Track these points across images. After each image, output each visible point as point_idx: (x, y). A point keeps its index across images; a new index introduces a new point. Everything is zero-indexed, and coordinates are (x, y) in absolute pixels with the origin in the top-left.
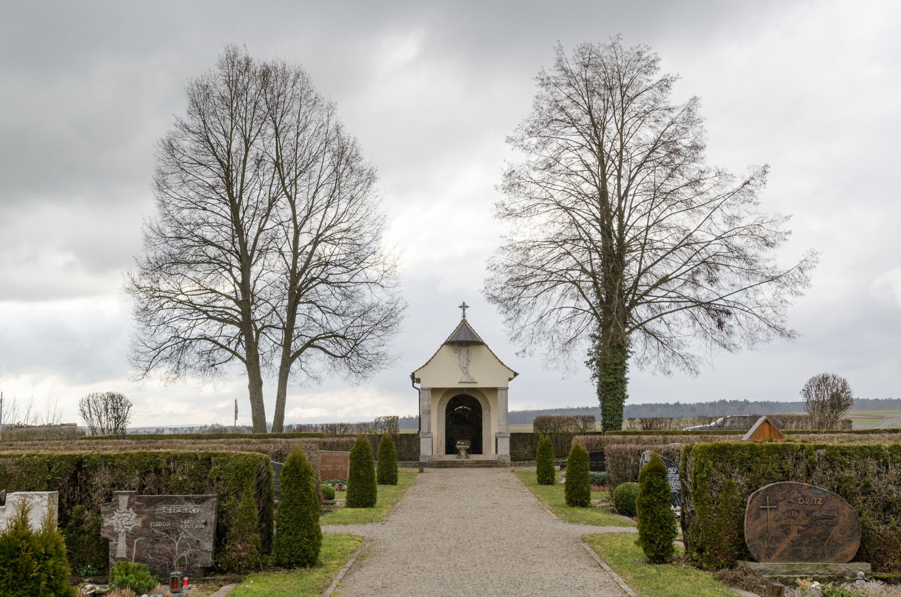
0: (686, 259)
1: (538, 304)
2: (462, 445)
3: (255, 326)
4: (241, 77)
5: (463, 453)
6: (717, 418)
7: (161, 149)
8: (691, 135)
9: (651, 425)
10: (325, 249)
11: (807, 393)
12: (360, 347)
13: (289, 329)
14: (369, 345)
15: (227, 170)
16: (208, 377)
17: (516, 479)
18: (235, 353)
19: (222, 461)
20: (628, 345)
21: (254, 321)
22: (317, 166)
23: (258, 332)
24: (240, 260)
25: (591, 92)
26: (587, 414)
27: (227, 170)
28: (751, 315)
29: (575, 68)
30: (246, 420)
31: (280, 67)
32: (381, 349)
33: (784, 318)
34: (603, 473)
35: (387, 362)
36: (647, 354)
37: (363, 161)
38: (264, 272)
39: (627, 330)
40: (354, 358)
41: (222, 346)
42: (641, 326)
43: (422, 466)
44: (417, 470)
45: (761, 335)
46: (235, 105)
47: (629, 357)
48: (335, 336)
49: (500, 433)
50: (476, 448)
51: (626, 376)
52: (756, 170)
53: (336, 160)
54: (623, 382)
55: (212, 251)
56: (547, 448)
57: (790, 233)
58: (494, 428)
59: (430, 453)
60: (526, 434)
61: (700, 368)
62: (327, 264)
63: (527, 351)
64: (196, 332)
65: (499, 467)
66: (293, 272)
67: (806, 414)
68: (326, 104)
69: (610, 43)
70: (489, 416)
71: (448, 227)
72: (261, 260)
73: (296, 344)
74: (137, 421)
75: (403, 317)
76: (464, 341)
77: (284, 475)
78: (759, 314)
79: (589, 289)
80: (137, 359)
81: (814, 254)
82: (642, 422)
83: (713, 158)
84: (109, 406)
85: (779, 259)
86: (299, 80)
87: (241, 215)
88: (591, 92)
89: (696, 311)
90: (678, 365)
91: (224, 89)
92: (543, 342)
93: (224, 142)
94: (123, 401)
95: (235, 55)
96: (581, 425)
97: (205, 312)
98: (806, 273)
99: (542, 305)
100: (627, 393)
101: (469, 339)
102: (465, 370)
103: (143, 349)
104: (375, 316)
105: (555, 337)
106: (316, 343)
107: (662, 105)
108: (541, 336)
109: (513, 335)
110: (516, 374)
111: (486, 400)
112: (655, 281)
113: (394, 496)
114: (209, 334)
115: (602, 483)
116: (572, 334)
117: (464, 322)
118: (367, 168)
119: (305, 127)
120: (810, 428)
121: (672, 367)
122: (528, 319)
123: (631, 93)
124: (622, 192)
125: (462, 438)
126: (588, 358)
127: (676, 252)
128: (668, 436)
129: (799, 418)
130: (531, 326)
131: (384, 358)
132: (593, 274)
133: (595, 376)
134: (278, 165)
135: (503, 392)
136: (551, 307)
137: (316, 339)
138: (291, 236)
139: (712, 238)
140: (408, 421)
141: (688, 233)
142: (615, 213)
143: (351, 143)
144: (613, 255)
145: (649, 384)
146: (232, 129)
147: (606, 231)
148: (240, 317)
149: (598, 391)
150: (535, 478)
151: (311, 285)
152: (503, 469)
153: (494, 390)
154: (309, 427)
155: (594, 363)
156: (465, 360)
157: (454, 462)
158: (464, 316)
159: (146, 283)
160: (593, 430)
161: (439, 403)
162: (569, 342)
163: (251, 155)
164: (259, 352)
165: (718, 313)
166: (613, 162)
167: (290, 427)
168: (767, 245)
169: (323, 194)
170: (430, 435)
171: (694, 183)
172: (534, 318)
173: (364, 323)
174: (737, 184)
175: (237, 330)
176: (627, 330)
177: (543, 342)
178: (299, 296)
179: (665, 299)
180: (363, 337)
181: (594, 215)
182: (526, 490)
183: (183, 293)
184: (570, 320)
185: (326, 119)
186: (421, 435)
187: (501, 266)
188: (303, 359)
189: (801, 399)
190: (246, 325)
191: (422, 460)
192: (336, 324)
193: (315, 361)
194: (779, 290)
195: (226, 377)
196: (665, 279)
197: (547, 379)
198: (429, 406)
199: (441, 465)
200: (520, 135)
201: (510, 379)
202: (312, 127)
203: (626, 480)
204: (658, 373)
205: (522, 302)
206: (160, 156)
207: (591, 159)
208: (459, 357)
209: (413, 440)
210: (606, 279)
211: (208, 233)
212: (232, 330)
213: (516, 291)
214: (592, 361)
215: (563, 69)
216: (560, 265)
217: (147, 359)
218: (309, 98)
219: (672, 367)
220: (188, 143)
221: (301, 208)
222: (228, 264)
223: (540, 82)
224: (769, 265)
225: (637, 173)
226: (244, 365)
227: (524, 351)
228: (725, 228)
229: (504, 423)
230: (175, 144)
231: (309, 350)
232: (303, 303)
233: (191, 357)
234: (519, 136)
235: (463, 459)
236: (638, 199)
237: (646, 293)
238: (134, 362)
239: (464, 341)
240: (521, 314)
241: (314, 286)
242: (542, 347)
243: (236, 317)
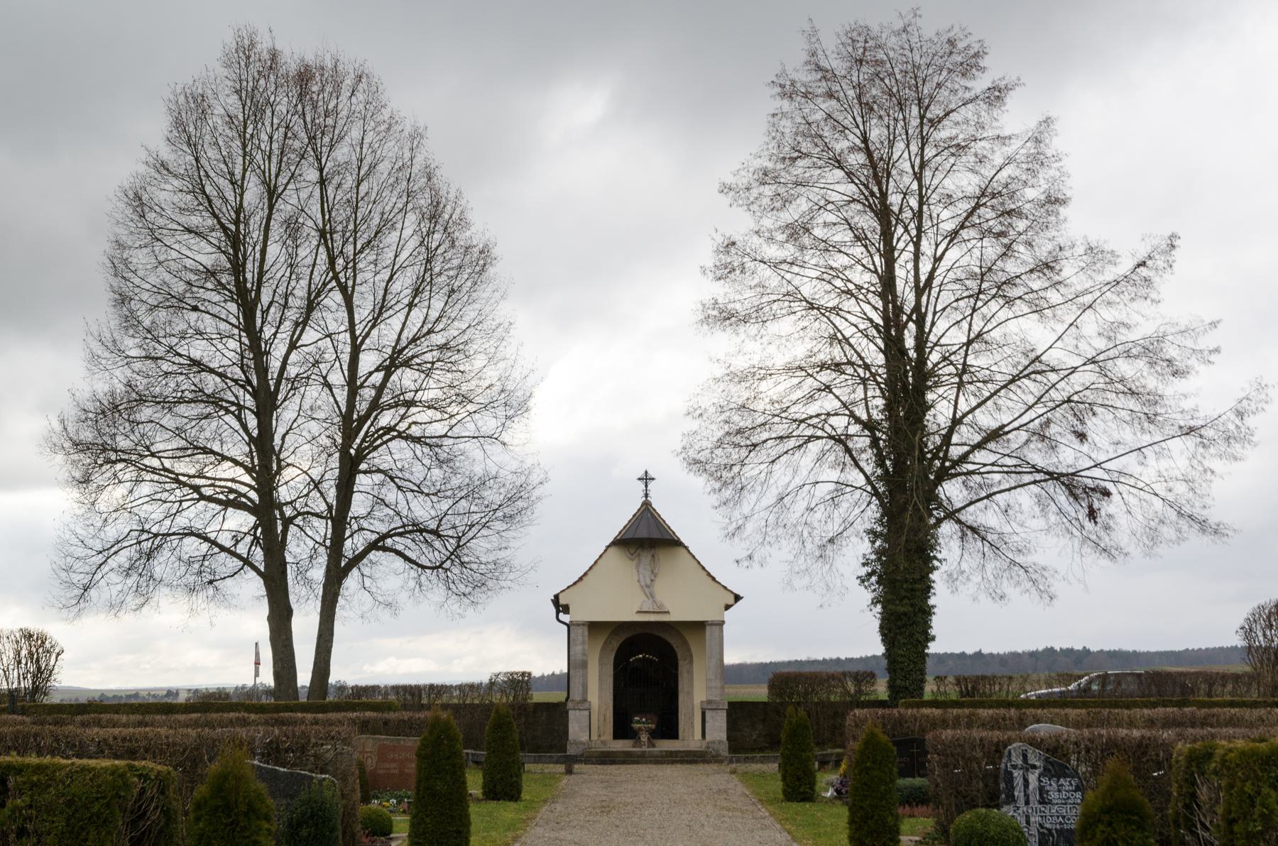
0: (1031, 400)
1: (775, 476)
2: (641, 723)
3: (282, 513)
4: (262, 82)
5: (644, 738)
6: (1080, 677)
7: (122, 205)
8: (1042, 182)
9: (973, 688)
10: (405, 378)
11: (1248, 632)
12: (466, 551)
13: (339, 517)
14: (481, 547)
15: (236, 241)
16: (200, 600)
17: (741, 788)
18: (247, 562)
19: (34, 785)
20: (932, 548)
21: (280, 506)
22: (392, 238)
23: (288, 522)
24: (254, 395)
25: (867, 108)
26: (861, 668)
27: (236, 241)
28: (1147, 496)
29: (839, 66)
30: (267, 678)
31: (329, 64)
32: (502, 554)
33: (1208, 501)
34: (918, 781)
35: (511, 576)
36: (964, 566)
37: (473, 229)
38: (300, 421)
39: (932, 521)
40: (456, 570)
41: (223, 549)
42: (952, 515)
43: (569, 762)
44: (561, 768)
45: (1167, 532)
46: (250, 130)
47: (936, 568)
48: (421, 531)
49: (709, 702)
50: (668, 727)
51: (931, 602)
52: (1155, 242)
53: (425, 227)
54: (926, 612)
55: (211, 383)
56: (790, 721)
57: (1217, 350)
58: (698, 691)
59: (585, 738)
60: (755, 704)
61: (1057, 587)
62: (410, 404)
63: (756, 557)
64: (181, 521)
65: (708, 762)
66: (346, 418)
67: (1248, 669)
68: (408, 129)
69: (899, 25)
70: (690, 672)
71: (626, 381)
72: (297, 399)
73: (353, 544)
74: (77, 675)
75: (539, 498)
76: (647, 539)
77: (198, 819)
78: (1162, 493)
79: (864, 451)
80: (68, 569)
81: (1261, 387)
82: (958, 682)
83: (1076, 225)
84: (24, 652)
85: (1203, 392)
86: (361, 87)
87: (259, 322)
88: (867, 108)
89: (1050, 486)
90: (1018, 583)
91: (233, 103)
92: (784, 542)
93: (230, 195)
94: (47, 645)
95: (252, 45)
96: (851, 687)
97: (196, 489)
98: (1250, 421)
99: (782, 476)
100: (933, 632)
101: (656, 535)
102: (648, 590)
103: (80, 552)
104: (492, 496)
105: (806, 534)
106: (389, 542)
107: (990, 133)
108: (780, 531)
109: (732, 528)
110: (737, 598)
111: (685, 643)
112: (977, 438)
113: (511, 827)
114: (198, 525)
115: (917, 799)
116: (834, 528)
117: (646, 507)
118: (478, 241)
119: (372, 167)
120: (1254, 696)
121: (1007, 587)
122: (757, 503)
123: (935, 111)
124: (923, 278)
125: (641, 712)
126: (864, 571)
127: (1012, 387)
128: (1028, 711)
129: (1236, 678)
130: (764, 514)
131: (506, 570)
132: (870, 425)
133: (874, 603)
134: (324, 235)
135: (716, 629)
136: (798, 481)
137: (384, 537)
138: (346, 358)
139: (1077, 362)
140: (550, 681)
141: (1032, 356)
142: (910, 318)
143: (452, 197)
144: (907, 383)
145: (971, 618)
146: (245, 170)
147: (893, 348)
148: (254, 495)
149: (881, 627)
150: (778, 786)
151: (379, 442)
152: (715, 767)
153: (700, 626)
154: (374, 689)
155: (874, 579)
156: (648, 573)
158: (646, 495)
159: (87, 435)
160: (872, 697)
161: (603, 649)
162: (831, 541)
163: (278, 217)
164: (289, 559)
165: (1084, 493)
166: (906, 230)
167: (341, 688)
168: (1175, 374)
169: (403, 285)
170: (586, 705)
171: (1045, 267)
172: (770, 498)
173: (473, 508)
174: (1125, 266)
175: (252, 520)
176: (932, 521)
177: (784, 542)
178: (360, 456)
179: (996, 469)
180: (471, 534)
181: (871, 321)
182: (764, 812)
183: (153, 455)
184: (833, 500)
185: (407, 155)
186: (570, 705)
187: (712, 410)
188: (366, 571)
189: (1238, 641)
190: (267, 511)
191: (571, 751)
192: (422, 510)
193: (386, 572)
194: (1201, 450)
195: (234, 602)
196: (995, 435)
197: (795, 604)
198: (584, 654)
199: (606, 758)
200: (745, 181)
201: (728, 607)
202: (384, 167)
203: (973, 805)
204: (982, 597)
205: (750, 471)
206: (119, 216)
207: (868, 222)
208: (638, 567)
209: (556, 714)
210: (896, 433)
211: (198, 349)
212: (241, 521)
213: (735, 455)
214: (870, 575)
215: (819, 68)
216: (813, 409)
217: (87, 569)
218: (379, 118)
219: (1007, 587)
220: (167, 195)
221: (363, 312)
222: (233, 403)
223: (779, 90)
224: (1187, 404)
225: (946, 250)
226: (262, 581)
227: (750, 557)
228: (1101, 344)
229: (717, 683)
230: (145, 197)
231: (373, 555)
232: (365, 472)
233: (163, 565)
234: (743, 181)
235: (645, 749)
236: (946, 298)
237: (964, 458)
238: (63, 574)
239: (647, 539)
240: (745, 492)
241: (385, 442)
242: (782, 553)
243: (245, 496)
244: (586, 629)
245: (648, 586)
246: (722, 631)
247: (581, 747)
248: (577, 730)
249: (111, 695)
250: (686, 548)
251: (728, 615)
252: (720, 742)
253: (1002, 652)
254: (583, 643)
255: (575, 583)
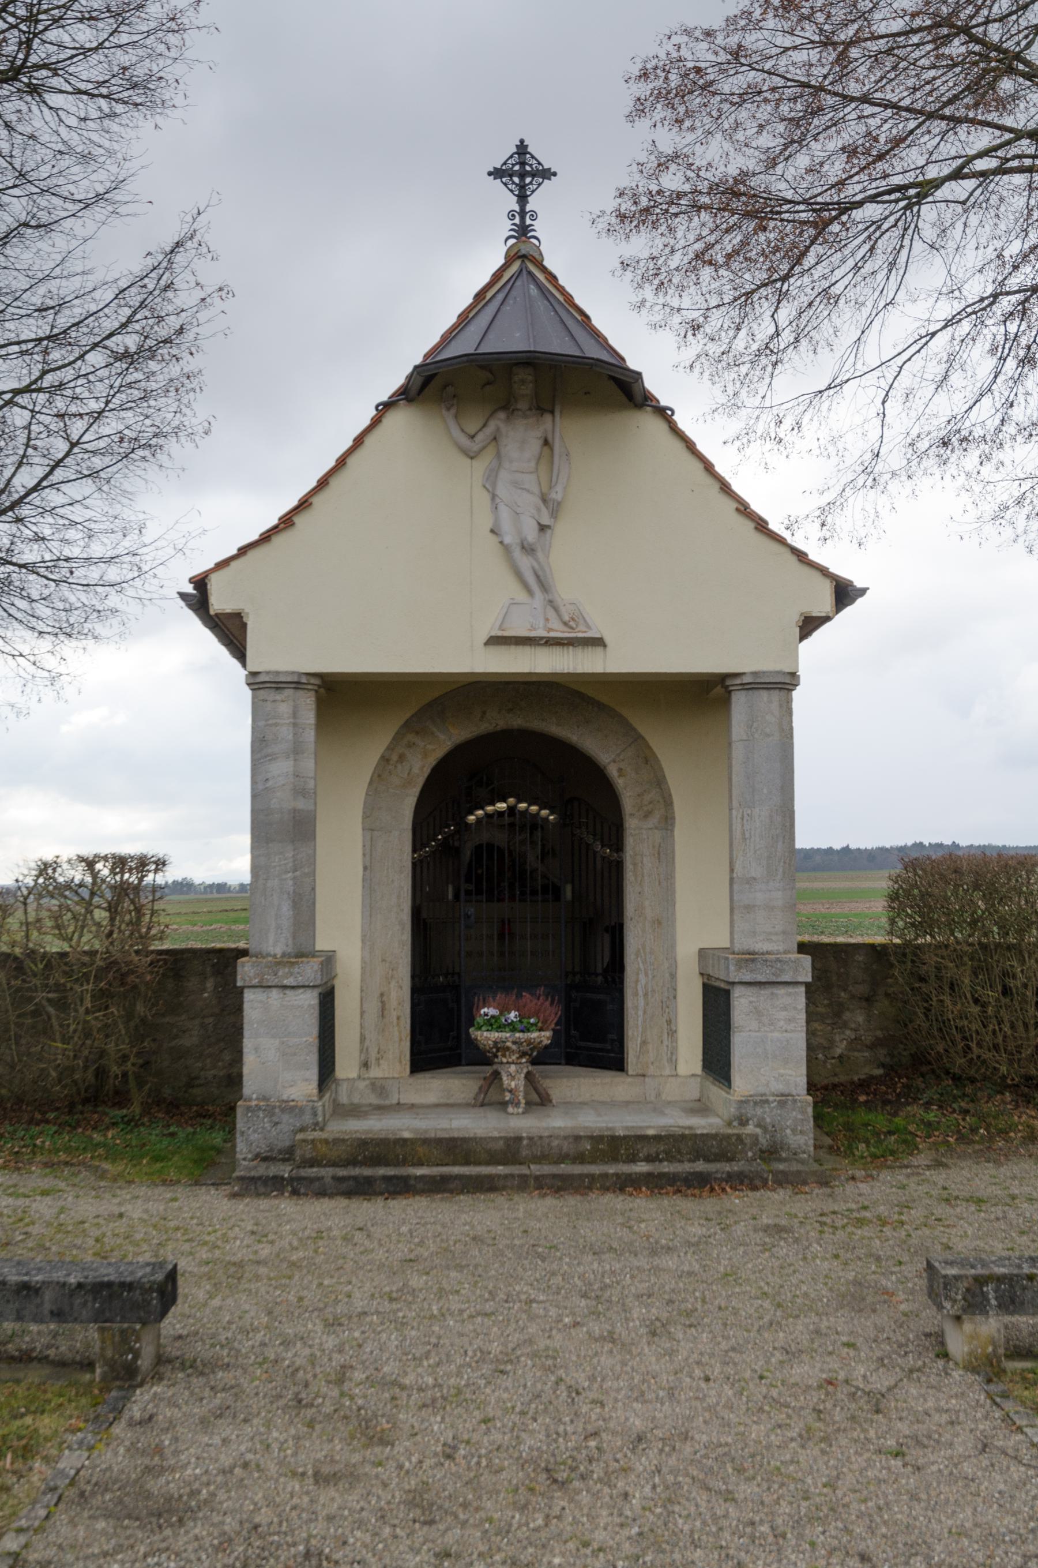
2: (504, 1025)
5: (514, 1076)
50: (592, 1034)
58: (689, 912)
70: (665, 855)
102: (527, 561)
110: (845, 594)
111: (647, 759)
117: (524, 259)
125: (508, 982)
153: (705, 695)
156: (529, 502)
157: (456, 1149)
158: (523, 231)
161: (379, 776)
198: (300, 792)
199: (376, 1170)
201: (809, 625)
239: (522, 382)
244: (307, 703)
245: (528, 549)
246: (789, 701)
247: (288, 1122)
248: (273, 1056)
249: (1012, 853)
250: (664, 413)
251: (813, 655)
252: (784, 1099)
253: (869, 847)
254: (297, 751)
255: (266, 538)
